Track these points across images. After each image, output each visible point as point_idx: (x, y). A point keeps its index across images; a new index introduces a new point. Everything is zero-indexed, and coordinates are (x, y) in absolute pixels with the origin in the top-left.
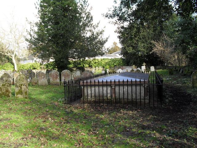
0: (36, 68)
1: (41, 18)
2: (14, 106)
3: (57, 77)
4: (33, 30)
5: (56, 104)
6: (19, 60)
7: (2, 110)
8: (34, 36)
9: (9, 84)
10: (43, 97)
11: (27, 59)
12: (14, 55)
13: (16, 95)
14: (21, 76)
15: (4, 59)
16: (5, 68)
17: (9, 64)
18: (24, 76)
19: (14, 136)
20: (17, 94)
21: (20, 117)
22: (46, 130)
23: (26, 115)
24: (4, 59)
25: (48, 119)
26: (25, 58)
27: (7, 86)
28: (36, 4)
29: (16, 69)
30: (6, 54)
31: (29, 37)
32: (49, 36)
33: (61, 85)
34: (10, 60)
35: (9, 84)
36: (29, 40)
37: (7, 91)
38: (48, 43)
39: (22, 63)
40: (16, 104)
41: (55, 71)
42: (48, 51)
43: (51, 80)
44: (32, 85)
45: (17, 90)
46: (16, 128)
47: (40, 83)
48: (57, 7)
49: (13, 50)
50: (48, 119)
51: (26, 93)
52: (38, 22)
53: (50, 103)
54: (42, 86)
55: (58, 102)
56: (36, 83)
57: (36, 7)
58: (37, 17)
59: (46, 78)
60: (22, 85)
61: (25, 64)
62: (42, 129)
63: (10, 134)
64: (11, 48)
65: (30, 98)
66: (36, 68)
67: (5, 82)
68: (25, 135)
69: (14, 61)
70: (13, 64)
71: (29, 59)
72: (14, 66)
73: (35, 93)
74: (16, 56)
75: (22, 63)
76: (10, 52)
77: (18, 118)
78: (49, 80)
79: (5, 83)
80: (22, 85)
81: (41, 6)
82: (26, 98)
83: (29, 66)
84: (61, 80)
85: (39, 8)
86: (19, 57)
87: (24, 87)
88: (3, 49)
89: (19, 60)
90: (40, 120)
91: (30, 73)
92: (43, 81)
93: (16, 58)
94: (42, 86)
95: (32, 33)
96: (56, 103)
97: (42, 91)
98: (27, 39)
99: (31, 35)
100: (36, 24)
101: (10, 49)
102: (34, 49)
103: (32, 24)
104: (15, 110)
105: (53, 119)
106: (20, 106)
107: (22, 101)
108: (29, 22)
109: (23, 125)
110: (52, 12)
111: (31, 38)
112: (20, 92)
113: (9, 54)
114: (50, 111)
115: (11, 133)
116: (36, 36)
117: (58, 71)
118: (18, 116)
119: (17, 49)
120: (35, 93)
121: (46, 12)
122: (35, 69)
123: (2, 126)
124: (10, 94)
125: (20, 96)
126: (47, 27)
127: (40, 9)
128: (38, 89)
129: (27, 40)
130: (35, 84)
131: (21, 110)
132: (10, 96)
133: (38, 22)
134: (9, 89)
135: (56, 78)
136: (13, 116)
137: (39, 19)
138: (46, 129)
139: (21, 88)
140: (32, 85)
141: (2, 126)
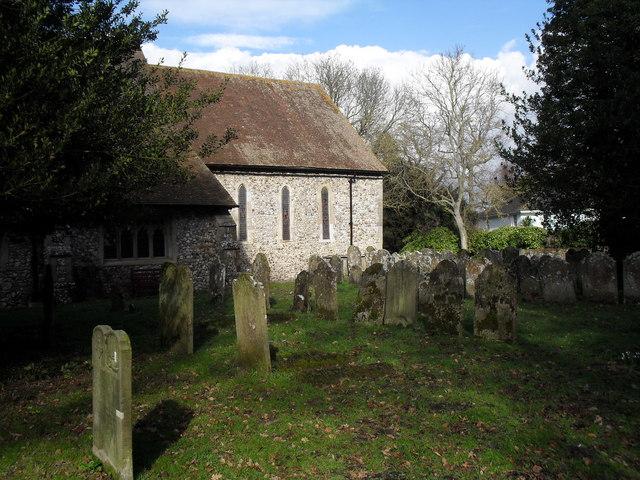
0: (528, 246)
1: (548, 80)
2: (472, 366)
3: (609, 277)
4: (522, 122)
5: (614, 369)
6: (472, 219)
7: (441, 376)
8: (528, 140)
9: (454, 293)
10: (564, 341)
11: (500, 213)
12: (459, 204)
13: (476, 330)
14: (495, 270)
15: (428, 215)
16: (433, 243)
17: (443, 231)
18: (503, 271)
19: (486, 463)
20: (480, 329)
21: (497, 404)
22: (590, 457)
23: (516, 399)
24: (428, 215)
25: (590, 416)
26: (493, 210)
27: (451, 300)
28: (530, 34)
29: (464, 246)
30: (435, 200)
31: (511, 145)
32: (577, 139)
33: (621, 302)
34: (446, 220)
35: (454, 293)
36: (513, 154)
37: (450, 316)
38: (573, 162)
39: (485, 228)
40: (478, 360)
41: (601, 255)
42: (576, 190)
43: (588, 285)
44: (524, 300)
45: (479, 314)
46: (487, 436)
47: (547, 292)
48: (602, 39)
49: (454, 187)
50: (591, 419)
51: (509, 324)
52: (541, 94)
53: (592, 365)
54: (557, 305)
55: (620, 362)
56: (534, 295)
57: (532, 48)
58: (536, 78)
59: (570, 279)
60: (495, 299)
61: (491, 230)
62: (574, 452)
63: (471, 454)
64: (451, 180)
65: (523, 344)
66: (528, 246)
67: (444, 289)
68: (519, 462)
69: (459, 221)
70: (456, 231)
71: (505, 216)
72: (459, 236)
73: (537, 326)
74: (463, 204)
75: (485, 228)
76: (446, 194)
77: (489, 404)
78: (578, 286)
79: (442, 292)
80: (495, 299)
81: (547, 41)
82: (508, 341)
83: (505, 236)
84: (620, 286)
85: (542, 49)
86: (473, 209)
87: (505, 305)
88: (425, 184)
89: (472, 219)
90: (565, 421)
91: (512, 259)
92: (559, 286)
93: (465, 211)
94: (557, 305)
95: (521, 131)
96: (613, 366)
97: (560, 320)
98: (504, 150)
99: (517, 138)
100: (534, 100)
101: (446, 183)
102: (524, 182)
103: (520, 103)
104: (478, 380)
105: (610, 422)
106: (493, 366)
107: (498, 351)
108: (511, 96)
109: (510, 430)
110: (586, 58)
111: (519, 149)
112: (491, 322)
113: (444, 201)
114: (597, 393)
115: (476, 451)
116: (533, 140)
117: (611, 253)
118: (491, 399)
119: (466, 184)
120: (537, 326)
121: (565, 57)
122: (524, 246)
123: (445, 425)
124: (459, 327)
125: (489, 335)
126: (570, 109)
127: (543, 53)
128: (542, 313)
129: (504, 154)
130: (532, 299)
131: (498, 380)
132: (457, 334)
133: (541, 94)
134: (457, 309)
135: (606, 279)
136: (475, 397)
137: (543, 84)
138: (589, 452)
139: (493, 308)
140: (524, 300)
141: (445, 425)
